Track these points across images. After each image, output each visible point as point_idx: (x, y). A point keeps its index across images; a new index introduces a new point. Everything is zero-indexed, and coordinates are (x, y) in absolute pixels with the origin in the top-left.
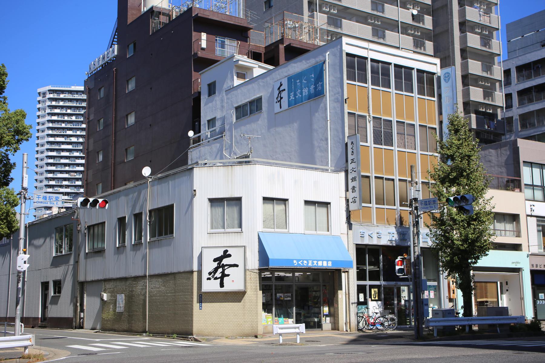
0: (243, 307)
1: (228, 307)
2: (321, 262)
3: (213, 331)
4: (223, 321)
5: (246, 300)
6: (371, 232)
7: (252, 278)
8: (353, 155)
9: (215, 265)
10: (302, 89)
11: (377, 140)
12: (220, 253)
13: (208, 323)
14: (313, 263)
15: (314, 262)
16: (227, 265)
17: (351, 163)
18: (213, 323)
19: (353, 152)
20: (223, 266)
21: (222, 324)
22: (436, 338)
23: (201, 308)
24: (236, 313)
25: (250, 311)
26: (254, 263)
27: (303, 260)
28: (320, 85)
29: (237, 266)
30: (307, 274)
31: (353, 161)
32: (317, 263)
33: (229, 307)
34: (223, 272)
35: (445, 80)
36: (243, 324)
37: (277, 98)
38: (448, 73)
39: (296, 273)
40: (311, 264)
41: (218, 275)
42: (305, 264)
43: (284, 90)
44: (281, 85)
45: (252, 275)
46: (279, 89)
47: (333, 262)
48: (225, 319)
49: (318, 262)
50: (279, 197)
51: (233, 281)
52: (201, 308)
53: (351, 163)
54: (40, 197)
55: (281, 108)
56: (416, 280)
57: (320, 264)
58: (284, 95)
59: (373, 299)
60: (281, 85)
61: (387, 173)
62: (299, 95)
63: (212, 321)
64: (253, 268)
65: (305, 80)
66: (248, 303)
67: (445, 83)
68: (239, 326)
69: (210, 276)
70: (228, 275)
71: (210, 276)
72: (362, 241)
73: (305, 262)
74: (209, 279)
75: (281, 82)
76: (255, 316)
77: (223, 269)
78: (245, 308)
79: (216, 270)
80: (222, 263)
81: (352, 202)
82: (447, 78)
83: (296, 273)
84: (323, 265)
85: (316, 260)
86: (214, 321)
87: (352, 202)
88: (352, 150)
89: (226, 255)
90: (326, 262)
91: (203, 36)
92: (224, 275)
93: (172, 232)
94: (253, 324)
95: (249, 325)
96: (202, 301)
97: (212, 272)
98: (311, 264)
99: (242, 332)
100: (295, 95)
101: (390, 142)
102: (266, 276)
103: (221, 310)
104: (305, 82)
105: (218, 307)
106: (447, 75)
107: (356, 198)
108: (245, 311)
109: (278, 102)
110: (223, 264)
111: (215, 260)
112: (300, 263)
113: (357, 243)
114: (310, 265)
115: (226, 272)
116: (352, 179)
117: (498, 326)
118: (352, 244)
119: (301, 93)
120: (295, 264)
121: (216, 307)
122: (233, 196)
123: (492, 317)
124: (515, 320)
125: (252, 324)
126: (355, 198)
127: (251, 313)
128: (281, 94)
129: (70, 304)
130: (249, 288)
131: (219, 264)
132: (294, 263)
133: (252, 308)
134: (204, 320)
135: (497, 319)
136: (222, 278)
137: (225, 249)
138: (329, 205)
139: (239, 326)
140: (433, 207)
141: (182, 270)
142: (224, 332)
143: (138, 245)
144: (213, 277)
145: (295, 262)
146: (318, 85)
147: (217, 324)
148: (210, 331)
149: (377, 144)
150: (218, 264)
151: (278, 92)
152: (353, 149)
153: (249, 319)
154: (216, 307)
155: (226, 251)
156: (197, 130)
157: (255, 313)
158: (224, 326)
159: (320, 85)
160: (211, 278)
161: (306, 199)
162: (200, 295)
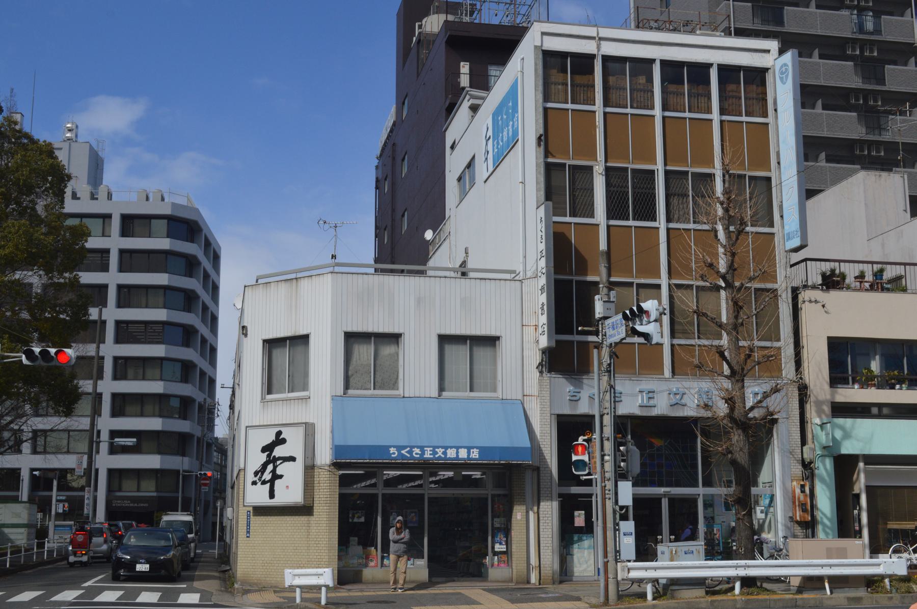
0: (307, 534)
3: (263, 576)
9: (263, 457)
12: (271, 438)
14: (435, 453)
15: (436, 450)
16: (279, 458)
20: (275, 459)
27: (412, 447)
29: (292, 459)
32: (445, 453)
34: (274, 471)
35: (781, 79)
40: (430, 454)
41: (267, 476)
42: (416, 454)
45: (321, 476)
47: (483, 450)
50: (381, 330)
52: (248, 535)
57: (451, 453)
61: (641, 272)
64: (323, 463)
67: (782, 84)
70: (281, 477)
73: (417, 451)
74: (254, 483)
77: (274, 465)
79: (264, 467)
80: (273, 455)
85: (442, 447)
89: (279, 440)
90: (466, 450)
91: (463, 67)
92: (276, 477)
98: (430, 454)
103: (275, 539)
106: (784, 69)
108: (310, 542)
111: (264, 450)
112: (403, 452)
113: (561, 412)
114: (428, 455)
120: (393, 456)
122: (297, 334)
123: (808, 561)
124: (645, 571)
131: (269, 456)
132: (391, 452)
135: (822, 566)
136: (272, 482)
137: (278, 429)
138: (497, 342)
142: (279, 579)
144: (260, 479)
145: (392, 450)
148: (259, 576)
149: (637, 220)
153: (315, 557)
155: (279, 433)
157: (323, 545)
158: (279, 568)
160: (258, 481)
161: (443, 332)
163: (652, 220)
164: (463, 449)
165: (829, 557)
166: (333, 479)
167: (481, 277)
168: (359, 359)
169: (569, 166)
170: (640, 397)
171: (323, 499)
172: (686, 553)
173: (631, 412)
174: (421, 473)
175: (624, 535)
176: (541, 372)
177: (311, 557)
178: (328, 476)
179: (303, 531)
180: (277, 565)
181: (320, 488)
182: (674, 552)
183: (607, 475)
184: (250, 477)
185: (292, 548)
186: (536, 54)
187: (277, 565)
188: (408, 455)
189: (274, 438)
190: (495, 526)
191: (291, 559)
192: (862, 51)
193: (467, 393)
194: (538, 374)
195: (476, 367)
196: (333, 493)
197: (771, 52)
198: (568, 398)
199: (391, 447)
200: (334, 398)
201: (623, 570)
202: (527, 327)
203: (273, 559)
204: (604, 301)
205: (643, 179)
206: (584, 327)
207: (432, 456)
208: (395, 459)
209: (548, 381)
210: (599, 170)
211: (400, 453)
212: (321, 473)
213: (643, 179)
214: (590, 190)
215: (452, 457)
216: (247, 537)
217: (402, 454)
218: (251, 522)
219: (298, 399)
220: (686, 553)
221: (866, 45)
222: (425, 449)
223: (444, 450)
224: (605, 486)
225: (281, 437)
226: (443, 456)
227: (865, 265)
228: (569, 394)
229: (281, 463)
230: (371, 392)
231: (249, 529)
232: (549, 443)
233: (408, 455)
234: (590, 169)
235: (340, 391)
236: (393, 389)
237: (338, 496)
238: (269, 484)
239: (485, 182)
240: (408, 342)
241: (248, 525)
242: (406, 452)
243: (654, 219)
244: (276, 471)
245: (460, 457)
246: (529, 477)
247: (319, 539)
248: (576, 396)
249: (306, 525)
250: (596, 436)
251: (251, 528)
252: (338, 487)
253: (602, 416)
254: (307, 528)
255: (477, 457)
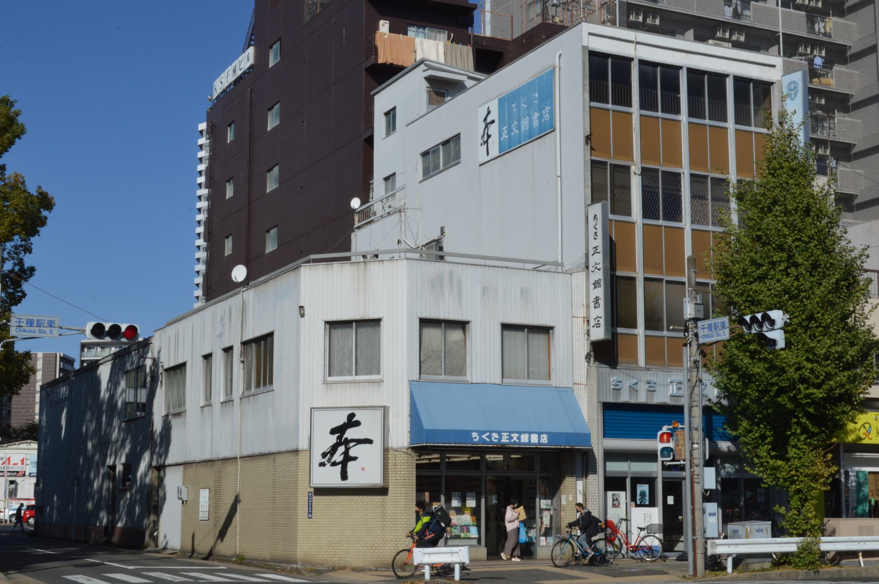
1: (356, 514)
2: (527, 435)
4: (347, 539)
5: (387, 503)
6: (635, 381)
7: (397, 464)
8: (596, 239)
9: (333, 439)
10: (519, 121)
11: (649, 211)
13: (322, 542)
14: (510, 438)
15: (512, 435)
16: (352, 440)
17: (593, 255)
18: (330, 542)
19: (596, 233)
20: (347, 442)
21: (345, 545)
22: (730, 576)
23: (310, 516)
24: (369, 526)
25: (393, 523)
26: (401, 437)
27: (491, 432)
28: (547, 111)
29: (368, 441)
30: (512, 456)
31: (596, 250)
32: (519, 438)
33: (357, 514)
34: (346, 453)
36: (381, 545)
37: (483, 136)
38: (794, 82)
39: (502, 459)
40: (507, 439)
41: (338, 457)
42: (495, 438)
43: (493, 122)
44: (489, 112)
45: (397, 459)
46: (485, 119)
47: (551, 435)
48: (351, 537)
49: (520, 435)
51: (363, 469)
52: (310, 516)
53: (593, 255)
54: (21, 320)
55: (488, 154)
56: (692, 470)
57: (524, 438)
58: (494, 130)
59: (638, 502)
60: (489, 112)
62: (514, 129)
63: (329, 539)
64: (400, 445)
65: (524, 103)
66: (391, 509)
68: (375, 548)
69: (325, 460)
70: (355, 459)
71: (325, 460)
72: (652, 398)
73: (495, 435)
74: (322, 464)
75: (488, 108)
76: (401, 531)
77: (346, 447)
78: (386, 517)
79: (334, 449)
80: (345, 436)
81: (593, 326)
82: (793, 92)
83: (502, 459)
84: (530, 440)
85: (517, 433)
86: (332, 539)
87: (593, 326)
88: (595, 230)
89: (352, 422)
91: (383, 25)
92: (348, 458)
93: (271, 382)
94: (399, 545)
95: (392, 548)
96: (312, 503)
97: (328, 453)
98: (507, 439)
99: (379, 559)
100: (510, 130)
101: (673, 212)
102: (433, 461)
104: (525, 106)
105: (339, 514)
106: (792, 86)
107: (601, 318)
108: (386, 523)
109: (484, 144)
110: (346, 439)
111: (333, 431)
112: (484, 436)
114: (505, 440)
115: (352, 453)
116: (594, 284)
117: (860, 554)
118: (596, 403)
119: (519, 128)
120: (475, 440)
121: (336, 514)
122: (367, 317)
123: (848, 537)
125: (398, 545)
126: (599, 319)
127: (395, 526)
128: (488, 129)
129: (415, 523)
130: (393, 481)
131: (339, 438)
132: (473, 436)
133: (398, 517)
134: (315, 536)
136: (344, 464)
137: (350, 412)
138: (551, 331)
139: (375, 548)
140: (722, 334)
141: (283, 449)
142: (348, 559)
143: (228, 402)
144: (329, 461)
145: (474, 435)
146: (544, 112)
147: (337, 545)
150: (338, 438)
151: (483, 125)
152: (596, 229)
154: (336, 514)
155: (351, 416)
156: (365, 200)
157: (402, 526)
159: (547, 111)
160: (326, 463)
162: (309, 493)
163: (654, 219)
164: (534, 435)
165: (861, 534)
166: (410, 461)
167: (463, 262)
168: (431, 345)
169: (610, 164)
170: (671, 387)
171: (400, 481)
172: (757, 531)
173: (663, 401)
174: (478, 458)
175: (710, 515)
176: (588, 362)
177: (387, 537)
178: (406, 458)
179: (376, 512)
180: (346, 545)
181: (397, 470)
182: (749, 531)
183: (696, 462)
184: (317, 458)
185: (363, 528)
186: (583, 54)
187: (346, 545)
188: (488, 440)
189: (345, 420)
190: (541, 507)
191: (363, 539)
192: (645, 19)
193: (525, 381)
194: (586, 364)
195: (530, 355)
196: (410, 475)
197: (776, 67)
198: (612, 387)
199: (473, 431)
200: (411, 382)
201: (712, 547)
202: (576, 319)
203: (341, 539)
204: (696, 304)
205: (671, 181)
206: (674, 326)
207: (508, 441)
208: (477, 443)
209: (596, 371)
210: (635, 169)
211: (481, 438)
212: (398, 456)
213: (671, 181)
214: (627, 188)
215: (525, 441)
216: (309, 518)
217: (483, 439)
218: (313, 503)
219: (369, 382)
220: (757, 531)
221: (650, 12)
222: (503, 434)
223: (518, 435)
224: (694, 471)
225: (354, 419)
226: (518, 441)
227: (873, 273)
228: (613, 383)
229: (355, 445)
230: (443, 377)
231: (311, 509)
232: (597, 429)
233: (488, 440)
234: (627, 169)
235: (416, 376)
236: (460, 375)
237: (415, 478)
238: (340, 466)
239: (480, 165)
240: (475, 329)
241: (310, 506)
242: (487, 437)
243: (680, 220)
244: (348, 453)
245: (532, 442)
246: (579, 459)
247: (402, 517)
248: (618, 385)
249: (381, 506)
250: (686, 426)
251: (313, 509)
252: (415, 470)
253: (691, 408)
254: (382, 509)
255: (546, 442)
